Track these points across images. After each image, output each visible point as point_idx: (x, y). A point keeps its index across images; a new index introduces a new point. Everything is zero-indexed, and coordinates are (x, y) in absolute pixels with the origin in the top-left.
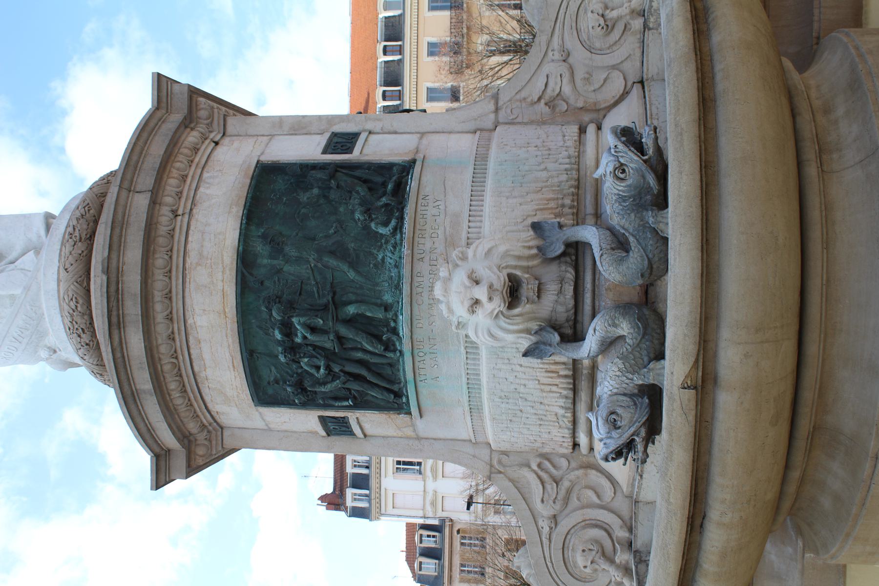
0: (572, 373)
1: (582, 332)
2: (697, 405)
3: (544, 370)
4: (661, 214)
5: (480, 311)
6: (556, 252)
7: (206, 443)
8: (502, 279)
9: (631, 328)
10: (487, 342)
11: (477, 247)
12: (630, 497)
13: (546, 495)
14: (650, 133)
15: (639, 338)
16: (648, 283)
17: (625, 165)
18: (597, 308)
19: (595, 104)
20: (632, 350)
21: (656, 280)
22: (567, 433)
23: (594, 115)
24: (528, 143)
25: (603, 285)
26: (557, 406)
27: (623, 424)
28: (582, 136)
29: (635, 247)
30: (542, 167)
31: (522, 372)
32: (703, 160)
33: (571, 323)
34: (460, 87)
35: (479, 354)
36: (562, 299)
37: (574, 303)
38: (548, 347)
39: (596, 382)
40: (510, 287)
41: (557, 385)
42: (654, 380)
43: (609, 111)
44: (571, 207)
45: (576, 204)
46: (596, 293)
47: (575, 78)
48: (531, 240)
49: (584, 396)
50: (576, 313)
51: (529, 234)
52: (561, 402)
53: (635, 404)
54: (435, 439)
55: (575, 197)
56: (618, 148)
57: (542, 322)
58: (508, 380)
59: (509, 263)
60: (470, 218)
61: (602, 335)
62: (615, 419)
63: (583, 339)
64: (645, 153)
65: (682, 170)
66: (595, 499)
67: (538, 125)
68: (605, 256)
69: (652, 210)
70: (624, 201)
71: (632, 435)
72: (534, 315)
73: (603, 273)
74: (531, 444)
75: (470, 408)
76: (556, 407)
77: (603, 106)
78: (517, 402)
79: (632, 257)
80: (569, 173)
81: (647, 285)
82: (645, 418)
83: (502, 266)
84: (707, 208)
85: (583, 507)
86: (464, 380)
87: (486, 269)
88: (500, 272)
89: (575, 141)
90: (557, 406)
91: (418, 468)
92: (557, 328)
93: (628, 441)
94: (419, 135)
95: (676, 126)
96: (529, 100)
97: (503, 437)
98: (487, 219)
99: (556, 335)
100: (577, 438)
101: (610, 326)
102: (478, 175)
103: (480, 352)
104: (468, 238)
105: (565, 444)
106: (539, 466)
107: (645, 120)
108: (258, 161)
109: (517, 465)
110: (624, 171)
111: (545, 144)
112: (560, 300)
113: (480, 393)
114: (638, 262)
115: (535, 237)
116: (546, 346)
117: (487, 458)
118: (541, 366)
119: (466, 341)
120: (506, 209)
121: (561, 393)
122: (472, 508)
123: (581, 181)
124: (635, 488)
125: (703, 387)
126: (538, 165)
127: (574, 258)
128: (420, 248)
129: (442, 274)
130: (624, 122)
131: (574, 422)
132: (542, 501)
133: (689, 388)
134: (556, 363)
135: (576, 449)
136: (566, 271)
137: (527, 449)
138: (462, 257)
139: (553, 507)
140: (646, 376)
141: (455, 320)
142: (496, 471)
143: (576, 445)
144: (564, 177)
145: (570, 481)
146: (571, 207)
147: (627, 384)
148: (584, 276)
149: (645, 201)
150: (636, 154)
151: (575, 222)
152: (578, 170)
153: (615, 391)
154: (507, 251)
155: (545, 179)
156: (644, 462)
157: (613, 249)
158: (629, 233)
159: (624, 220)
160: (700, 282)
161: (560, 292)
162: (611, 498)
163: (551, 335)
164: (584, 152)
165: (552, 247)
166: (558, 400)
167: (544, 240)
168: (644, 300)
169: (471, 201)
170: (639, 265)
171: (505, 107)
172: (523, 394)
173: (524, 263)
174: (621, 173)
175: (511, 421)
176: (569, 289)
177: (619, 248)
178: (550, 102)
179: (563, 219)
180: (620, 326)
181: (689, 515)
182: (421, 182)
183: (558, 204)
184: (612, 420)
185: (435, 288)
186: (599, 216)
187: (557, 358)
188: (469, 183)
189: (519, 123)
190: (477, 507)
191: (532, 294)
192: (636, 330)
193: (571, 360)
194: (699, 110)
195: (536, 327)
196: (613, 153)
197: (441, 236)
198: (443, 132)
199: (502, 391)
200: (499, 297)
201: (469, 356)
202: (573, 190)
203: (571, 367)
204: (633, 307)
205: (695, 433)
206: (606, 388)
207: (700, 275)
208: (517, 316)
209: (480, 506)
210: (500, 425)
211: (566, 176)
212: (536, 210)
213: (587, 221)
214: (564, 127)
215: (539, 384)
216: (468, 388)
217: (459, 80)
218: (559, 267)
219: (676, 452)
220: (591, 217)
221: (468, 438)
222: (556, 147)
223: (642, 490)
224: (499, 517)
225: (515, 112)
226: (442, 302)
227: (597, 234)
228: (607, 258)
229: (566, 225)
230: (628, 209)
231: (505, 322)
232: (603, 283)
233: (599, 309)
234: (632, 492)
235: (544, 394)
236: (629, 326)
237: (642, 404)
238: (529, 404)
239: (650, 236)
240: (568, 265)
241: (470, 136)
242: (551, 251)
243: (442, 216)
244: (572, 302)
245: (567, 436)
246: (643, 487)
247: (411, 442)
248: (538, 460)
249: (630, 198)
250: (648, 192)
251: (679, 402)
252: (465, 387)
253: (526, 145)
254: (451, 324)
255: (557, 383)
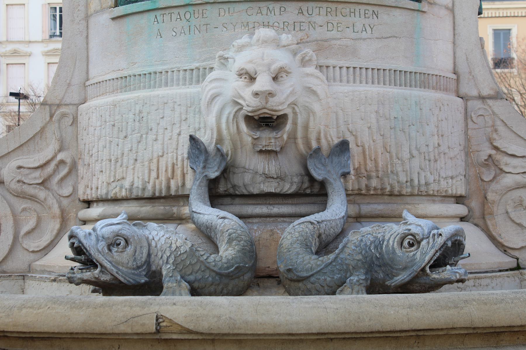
0: (173, 194)
1: (222, 205)
2: (137, 334)
3: (175, 161)
4: (362, 290)
5: (242, 82)
6: (315, 170)
8: (280, 108)
9: (228, 259)
10: (205, 93)
11: (317, 77)
12: (30, 269)
13: (27, 171)
14: (457, 275)
15: (215, 269)
16: (281, 277)
17: (419, 247)
18: (250, 220)
19: (491, 214)
20: (202, 262)
21: (284, 286)
22: (102, 192)
23: (477, 212)
24: (442, 136)
25: (277, 227)
26: (134, 178)
27: (115, 254)
28: (453, 199)
29: (322, 261)
30: (415, 153)
31: (171, 136)
32: (426, 334)
33: (231, 191)
34: (512, 68)
35: (191, 84)
36: (259, 179)
37: (255, 193)
38: (202, 165)
39: (164, 223)
40: (271, 118)
41: (158, 177)
42: (167, 288)
43: (483, 230)
44: (368, 187)
45: (372, 192)
46: (268, 219)
47: (521, 190)
48: (328, 141)
49: (146, 209)
50: (243, 196)
51: (334, 139)
52: (138, 184)
53: (138, 268)
54: (87, 37)
55: (379, 192)
56: (438, 237)
57: (231, 156)
58: (161, 120)
59: (299, 116)
60: (352, 69)
61: (218, 226)
62: (120, 244)
63: (213, 205)
64: (433, 269)
65: (414, 308)
66: (25, 229)
67: (465, 147)
68: (311, 227)
69: (366, 280)
70: (376, 247)
71: (102, 266)
72: (240, 147)
73: (291, 225)
74: (87, 150)
75: (126, 77)
76: (132, 178)
77: (489, 223)
78: (136, 131)
79: (310, 258)
80: (408, 184)
81: (278, 277)
82: (122, 279)
83: (296, 108)
84: (369, 338)
85: (14, 215)
86: (159, 68)
87: (291, 89)
88: (289, 105)
89: (446, 191)
90: (134, 178)
91: (58, 33)
92: (225, 175)
93: (94, 260)
94: (450, 5)
95: (466, 301)
96: (495, 136)
97: (94, 118)
98: (351, 88)
99: (217, 174)
100: (97, 205)
101: (230, 235)
102: (403, 77)
103: (193, 85)
104: (327, 67)
105: (88, 191)
106: (62, 162)
107: (473, 271)
109: (61, 136)
110: (411, 245)
111: (442, 155)
112: (258, 176)
113: (144, 87)
114: (305, 265)
115: (332, 145)
116: (203, 163)
117: (68, 100)
118: (180, 158)
119: (206, 69)
120: (363, 110)
121: (149, 183)
122: (13, 99)
123: (399, 198)
124: (41, 274)
125: (160, 341)
126: (416, 147)
127: (308, 191)
128: (314, 10)
129: (284, 36)
130: (469, 246)
131: (115, 200)
132: (20, 167)
133: (158, 324)
134: (184, 175)
135: (83, 203)
136: (292, 184)
137: (81, 147)
138: (305, 60)
139: (12, 180)
140: (171, 279)
141: (229, 54)
142: (53, 111)
143: (88, 203)
144: (403, 178)
145: (45, 199)
146: (368, 187)
147: (162, 257)
148: (287, 204)
149: (376, 272)
150: (431, 259)
151: (350, 192)
152: (412, 195)
153: (153, 244)
154: (314, 113)
155: (400, 156)
156: (71, 281)
157: (320, 236)
158: (339, 254)
159: (354, 248)
160: (282, 332)
161: (268, 177)
162: (27, 247)
163: (216, 168)
164: (434, 201)
165: (319, 166)
166: (140, 180)
167: (328, 157)
168: (262, 274)
169: (372, 69)
170: (301, 266)
171: (486, 107)
172: (146, 138)
173: (300, 134)
174: (409, 242)
175: (114, 125)
176: (271, 187)
177: (320, 243)
178: (493, 161)
179: (353, 177)
180: (230, 247)
181: (7, 332)
182: (393, 9)
183: (371, 171)
184: (118, 242)
185: (267, 29)
186: (358, 220)
187: (189, 177)
188: (393, 67)
189: (467, 125)
190: (14, 105)
191: (264, 143)
192: (225, 265)
193: (188, 193)
194: (484, 328)
195: (225, 150)
196: (433, 232)
197: (329, 35)
198: (454, 35)
199: (148, 113)
200: (259, 104)
201: (188, 72)
202: (388, 188)
203: (180, 193)
204: (253, 262)
205: (105, 334)
206: (156, 233)
207: (291, 332)
208: (238, 128)
209: (16, 108)
210: (108, 113)
211: (405, 180)
212: (363, 146)
213: (352, 207)
214: (463, 178)
215: (159, 157)
216: (150, 74)
217: (520, 67)
218: (297, 175)
219: (82, 313)
220: (357, 211)
221: (91, 76)
222: (439, 168)
223: (37, 282)
224: (4, 131)
225: (480, 120)
226: (251, 38)
227: (337, 217)
228: (309, 229)
229: (346, 181)
230: (366, 252)
231: (229, 114)
232: (279, 227)
233: (249, 222)
234: (36, 271)
235: (146, 163)
236: (230, 257)
237: (139, 275)
238: (135, 146)
239: (335, 277)
240: (300, 185)
241: (451, 67)
242: (315, 165)
243: (353, 35)
244: (256, 191)
245: (99, 193)
246: (42, 283)
247: (82, 8)
248: (69, 161)
249: (380, 254)
250: (388, 275)
251: (140, 313)
252: (152, 69)
253: (440, 133)
254: (225, 50)
255: (160, 178)
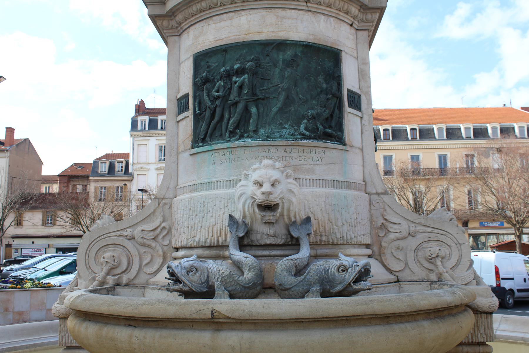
7: (170, 26)
62: (193, 271)
108: (341, 50)
184: (192, 270)
